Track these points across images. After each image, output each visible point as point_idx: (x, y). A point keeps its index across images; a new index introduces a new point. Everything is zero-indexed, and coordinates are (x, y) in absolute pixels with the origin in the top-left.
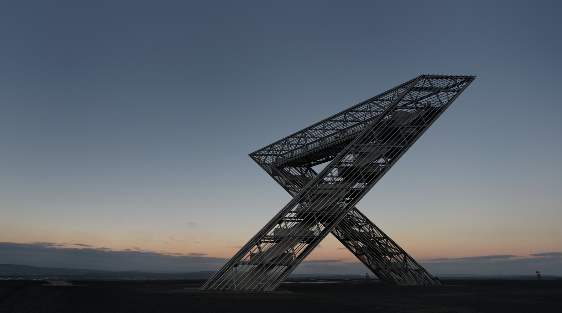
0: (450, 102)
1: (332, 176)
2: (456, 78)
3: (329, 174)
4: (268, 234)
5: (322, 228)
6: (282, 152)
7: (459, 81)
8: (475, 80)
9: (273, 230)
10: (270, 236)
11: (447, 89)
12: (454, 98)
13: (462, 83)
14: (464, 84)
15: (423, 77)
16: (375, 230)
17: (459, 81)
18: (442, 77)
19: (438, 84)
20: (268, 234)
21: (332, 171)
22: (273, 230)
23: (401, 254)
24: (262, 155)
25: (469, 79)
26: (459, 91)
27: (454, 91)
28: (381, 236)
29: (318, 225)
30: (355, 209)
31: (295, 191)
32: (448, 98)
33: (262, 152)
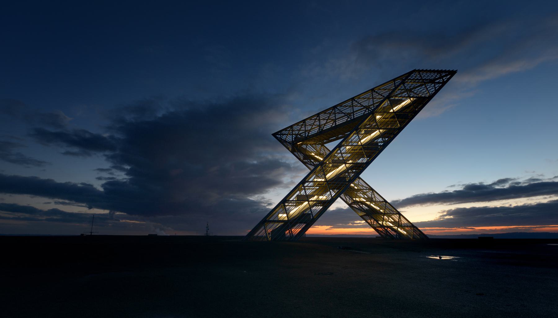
0: (437, 91)
1: (341, 153)
2: (442, 71)
3: (339, 152)
4: (291, 199)
5: (333, 194)
6: (301, 132)
7: (444, 74)
8: (84, 182)
9: (295, 195)
10: (293, 201)
11: (432, 81)
12: (440, 88)
13: (446, 76)
14: (448, 77)
15: (414, 71)
16: (375, 194)
17: (444, 74)
18: (430, 71)
19: (425, 76)
20: (291, 199)
21: (341, 149)
22: (295, 195)
23: (396, 214)
24: (283, 135)
25: (452, 73)
26: (444, 83)
27: (439, 83)
28: (382, 200)
29: (297, 169)
30: (360, 178)
31: (311, 165)
32: (435, 88)
33: (284, 132)
